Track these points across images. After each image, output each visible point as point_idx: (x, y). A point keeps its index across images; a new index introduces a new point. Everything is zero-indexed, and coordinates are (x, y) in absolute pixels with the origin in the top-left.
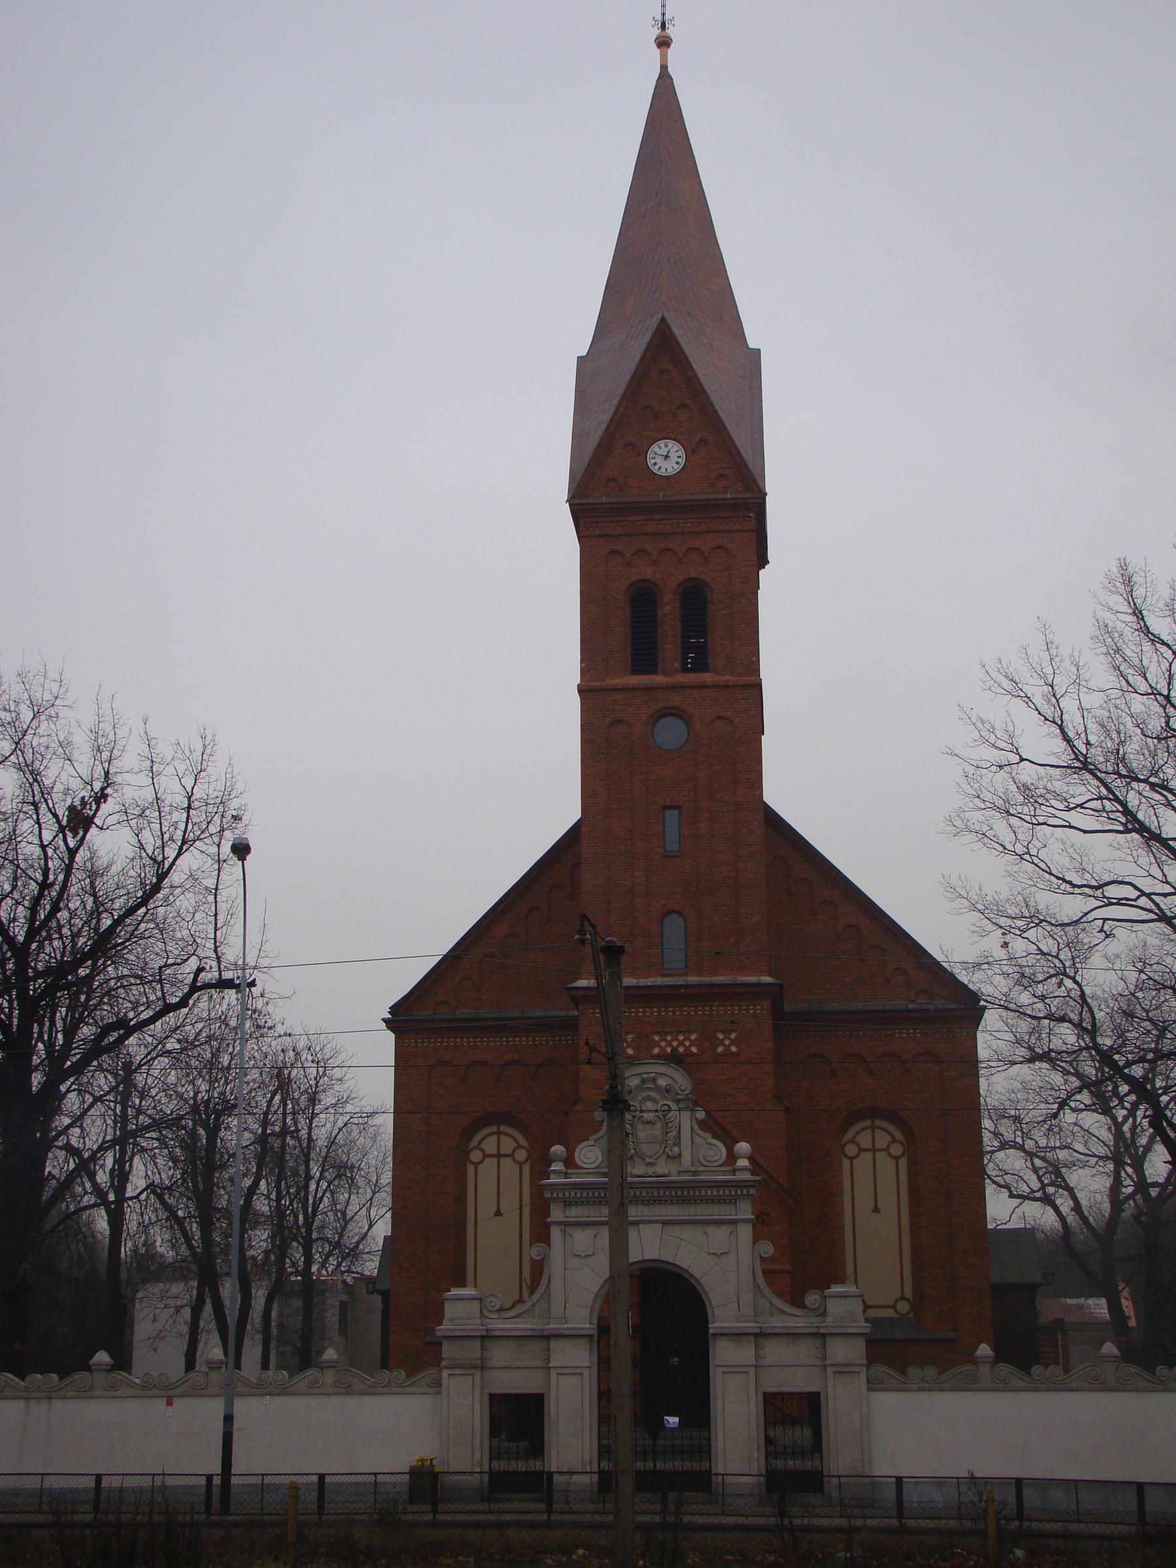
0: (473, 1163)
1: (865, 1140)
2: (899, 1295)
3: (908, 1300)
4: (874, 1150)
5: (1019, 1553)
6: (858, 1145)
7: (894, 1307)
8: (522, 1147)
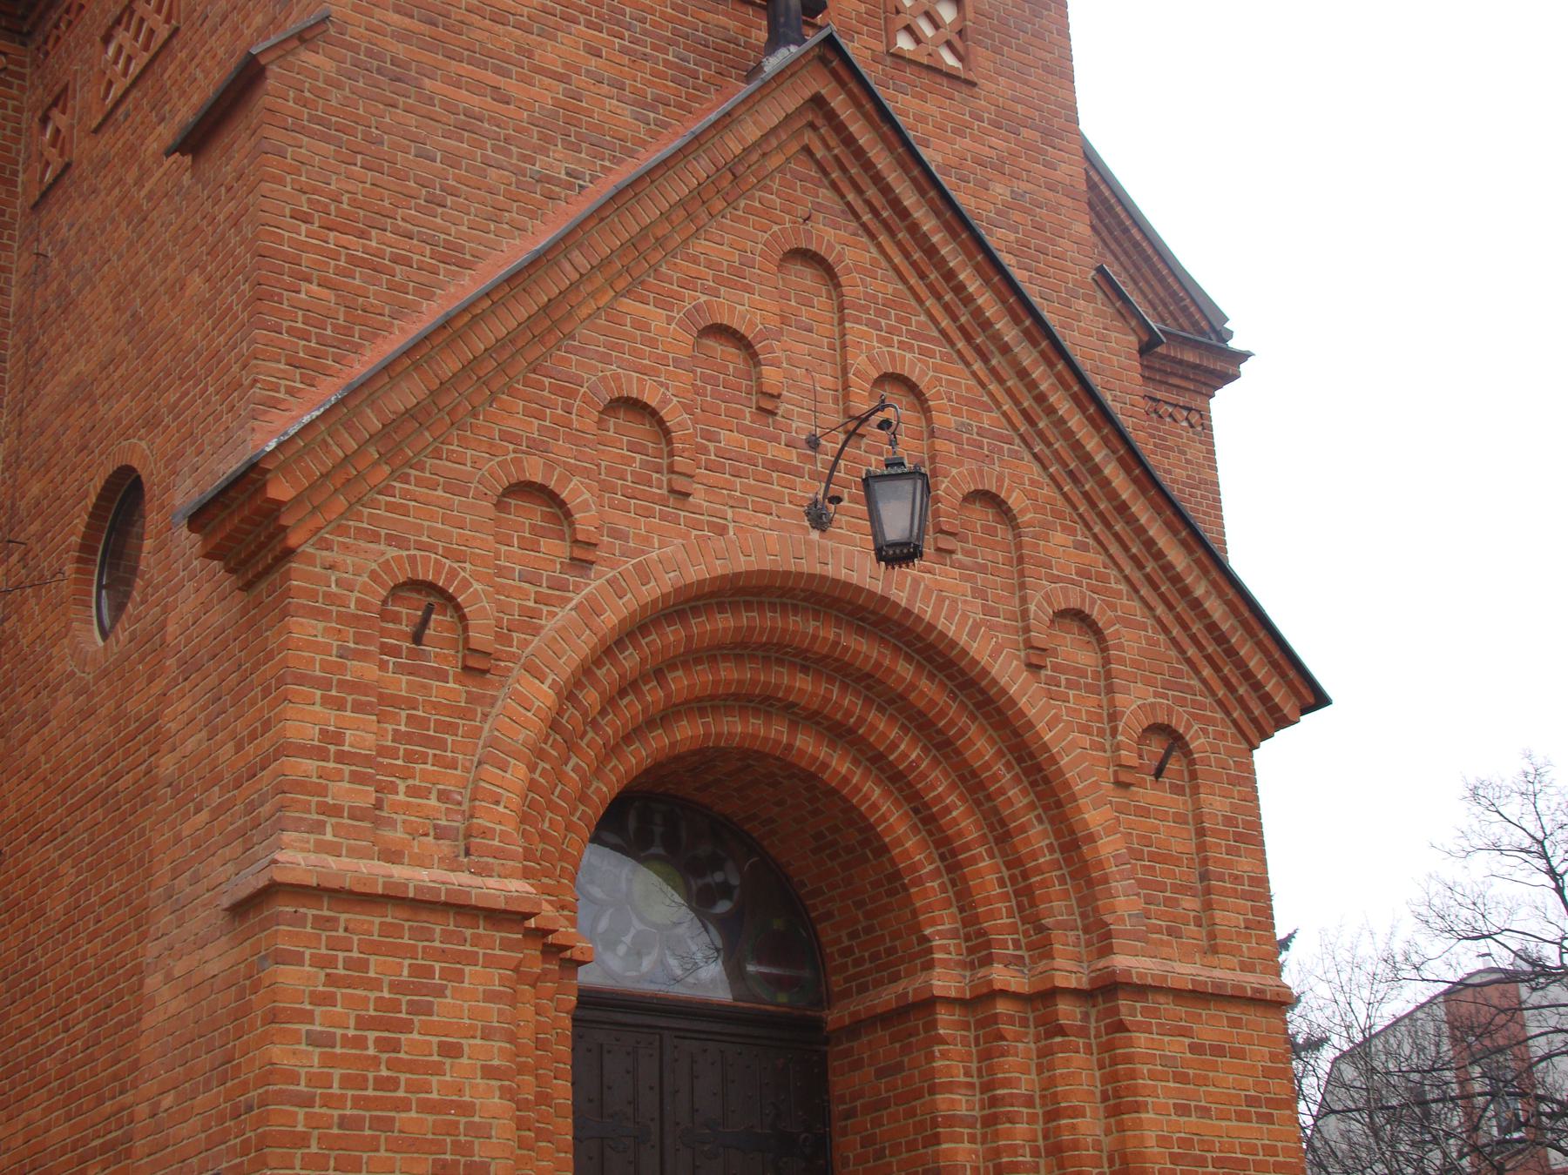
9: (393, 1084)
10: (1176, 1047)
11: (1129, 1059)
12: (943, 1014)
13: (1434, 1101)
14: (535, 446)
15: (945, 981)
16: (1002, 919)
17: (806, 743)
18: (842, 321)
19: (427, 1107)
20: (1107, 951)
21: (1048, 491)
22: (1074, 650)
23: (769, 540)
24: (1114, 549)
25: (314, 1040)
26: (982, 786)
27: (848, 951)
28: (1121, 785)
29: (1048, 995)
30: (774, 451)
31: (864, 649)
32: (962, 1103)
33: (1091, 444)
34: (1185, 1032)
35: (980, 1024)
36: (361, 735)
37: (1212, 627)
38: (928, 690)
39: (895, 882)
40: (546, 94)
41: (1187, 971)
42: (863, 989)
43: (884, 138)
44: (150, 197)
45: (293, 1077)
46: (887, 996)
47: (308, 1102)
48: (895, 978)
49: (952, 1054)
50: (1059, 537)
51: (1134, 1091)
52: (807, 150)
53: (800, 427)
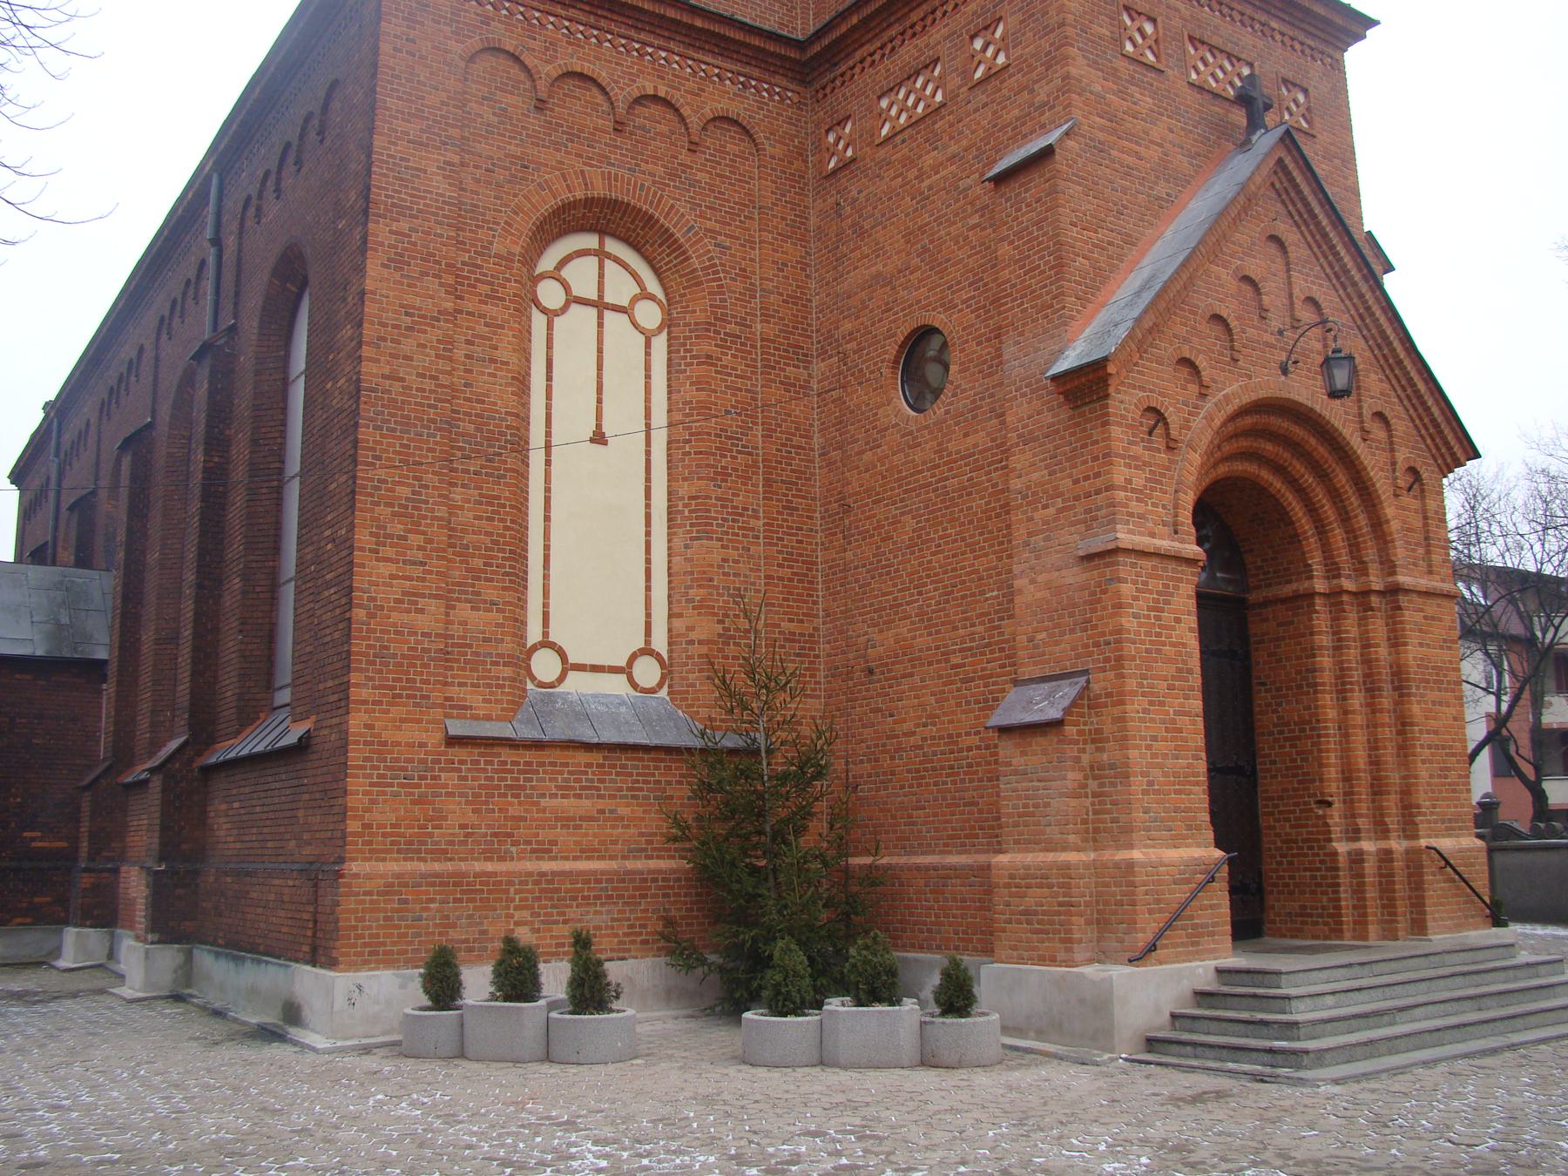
0: (544, 311)
1: (582, 276)
2: (640, 643)
3: (658, 657)
4: (600, 305)
5: (1144, 1160)
6: (566, 287)
7: (626, 670)
8: (652, 298)
10: (1418, 617)
11: (1402, 622)
12: (1318, 601)
14: (1186, 340)
15: (1320, 585)
16: (1343, 557)
17: (1266, 475)
18: (1288, 271)
19: (1173, 645)
20: (1393, 573)
21: (1368, 354)
22: (1379, 433)
23: (1266, 383)
24: (1394, 381)
26: (1339, 495)
27: (1258, 568)
28: (1396, 496)
29: (1366, 593)
30: (1267, 337)
31: (1299, 432)
32: (1324, 640)
33: (1389, 331)
34: (1421, 610)
35: (1332, 605)
36: (1138, 482)
37: (1433, 420)
38: (1322, 451)
39: (1295, 539)
40: (1154, 153)
41: (1424, 583)
42: (1270, 585)
43: (1306, 178)
44: (930, 188)
45: (1129, 632)
46: (1288, 590)
48: (1289, 582)
49: (1321, 620)
50: (1373, 376)
51: (1404, 636)
52: (1273, 184)
53: (1275, 324)
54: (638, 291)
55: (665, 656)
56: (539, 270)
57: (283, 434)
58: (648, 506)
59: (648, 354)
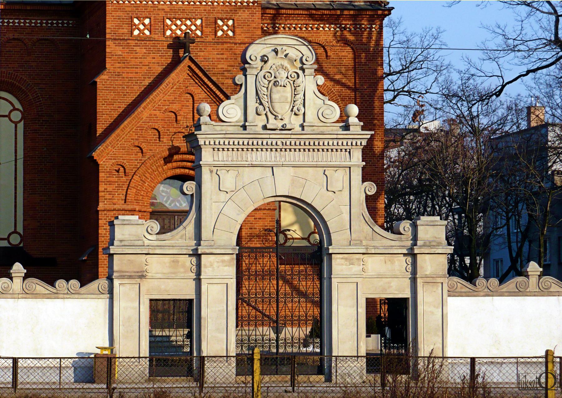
3: (19, 234)
8: (18, 110)
9: (36, 95)
13: (529, 121)
25: (104, 229)
47: (104, 237)
54: (12, 108)
55: (22, 233)
56: (22, 122)
57: (24, 185)
58: (16, 183)
59: (16, 130)
